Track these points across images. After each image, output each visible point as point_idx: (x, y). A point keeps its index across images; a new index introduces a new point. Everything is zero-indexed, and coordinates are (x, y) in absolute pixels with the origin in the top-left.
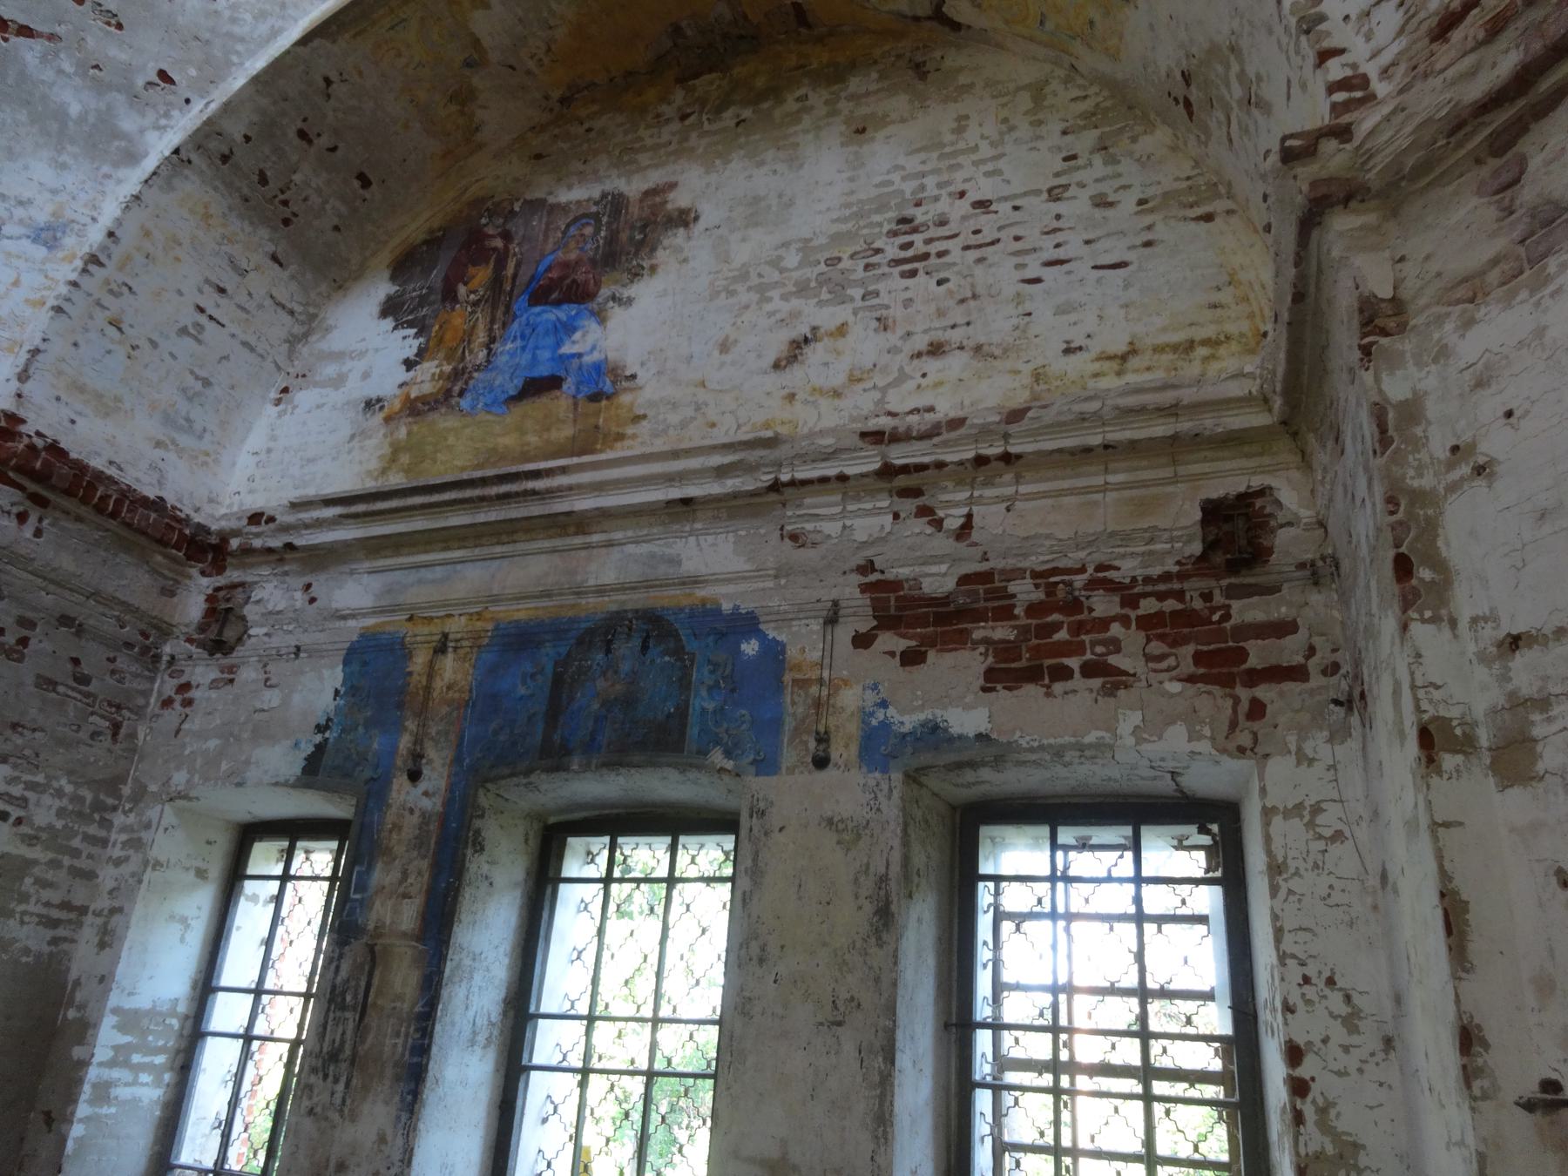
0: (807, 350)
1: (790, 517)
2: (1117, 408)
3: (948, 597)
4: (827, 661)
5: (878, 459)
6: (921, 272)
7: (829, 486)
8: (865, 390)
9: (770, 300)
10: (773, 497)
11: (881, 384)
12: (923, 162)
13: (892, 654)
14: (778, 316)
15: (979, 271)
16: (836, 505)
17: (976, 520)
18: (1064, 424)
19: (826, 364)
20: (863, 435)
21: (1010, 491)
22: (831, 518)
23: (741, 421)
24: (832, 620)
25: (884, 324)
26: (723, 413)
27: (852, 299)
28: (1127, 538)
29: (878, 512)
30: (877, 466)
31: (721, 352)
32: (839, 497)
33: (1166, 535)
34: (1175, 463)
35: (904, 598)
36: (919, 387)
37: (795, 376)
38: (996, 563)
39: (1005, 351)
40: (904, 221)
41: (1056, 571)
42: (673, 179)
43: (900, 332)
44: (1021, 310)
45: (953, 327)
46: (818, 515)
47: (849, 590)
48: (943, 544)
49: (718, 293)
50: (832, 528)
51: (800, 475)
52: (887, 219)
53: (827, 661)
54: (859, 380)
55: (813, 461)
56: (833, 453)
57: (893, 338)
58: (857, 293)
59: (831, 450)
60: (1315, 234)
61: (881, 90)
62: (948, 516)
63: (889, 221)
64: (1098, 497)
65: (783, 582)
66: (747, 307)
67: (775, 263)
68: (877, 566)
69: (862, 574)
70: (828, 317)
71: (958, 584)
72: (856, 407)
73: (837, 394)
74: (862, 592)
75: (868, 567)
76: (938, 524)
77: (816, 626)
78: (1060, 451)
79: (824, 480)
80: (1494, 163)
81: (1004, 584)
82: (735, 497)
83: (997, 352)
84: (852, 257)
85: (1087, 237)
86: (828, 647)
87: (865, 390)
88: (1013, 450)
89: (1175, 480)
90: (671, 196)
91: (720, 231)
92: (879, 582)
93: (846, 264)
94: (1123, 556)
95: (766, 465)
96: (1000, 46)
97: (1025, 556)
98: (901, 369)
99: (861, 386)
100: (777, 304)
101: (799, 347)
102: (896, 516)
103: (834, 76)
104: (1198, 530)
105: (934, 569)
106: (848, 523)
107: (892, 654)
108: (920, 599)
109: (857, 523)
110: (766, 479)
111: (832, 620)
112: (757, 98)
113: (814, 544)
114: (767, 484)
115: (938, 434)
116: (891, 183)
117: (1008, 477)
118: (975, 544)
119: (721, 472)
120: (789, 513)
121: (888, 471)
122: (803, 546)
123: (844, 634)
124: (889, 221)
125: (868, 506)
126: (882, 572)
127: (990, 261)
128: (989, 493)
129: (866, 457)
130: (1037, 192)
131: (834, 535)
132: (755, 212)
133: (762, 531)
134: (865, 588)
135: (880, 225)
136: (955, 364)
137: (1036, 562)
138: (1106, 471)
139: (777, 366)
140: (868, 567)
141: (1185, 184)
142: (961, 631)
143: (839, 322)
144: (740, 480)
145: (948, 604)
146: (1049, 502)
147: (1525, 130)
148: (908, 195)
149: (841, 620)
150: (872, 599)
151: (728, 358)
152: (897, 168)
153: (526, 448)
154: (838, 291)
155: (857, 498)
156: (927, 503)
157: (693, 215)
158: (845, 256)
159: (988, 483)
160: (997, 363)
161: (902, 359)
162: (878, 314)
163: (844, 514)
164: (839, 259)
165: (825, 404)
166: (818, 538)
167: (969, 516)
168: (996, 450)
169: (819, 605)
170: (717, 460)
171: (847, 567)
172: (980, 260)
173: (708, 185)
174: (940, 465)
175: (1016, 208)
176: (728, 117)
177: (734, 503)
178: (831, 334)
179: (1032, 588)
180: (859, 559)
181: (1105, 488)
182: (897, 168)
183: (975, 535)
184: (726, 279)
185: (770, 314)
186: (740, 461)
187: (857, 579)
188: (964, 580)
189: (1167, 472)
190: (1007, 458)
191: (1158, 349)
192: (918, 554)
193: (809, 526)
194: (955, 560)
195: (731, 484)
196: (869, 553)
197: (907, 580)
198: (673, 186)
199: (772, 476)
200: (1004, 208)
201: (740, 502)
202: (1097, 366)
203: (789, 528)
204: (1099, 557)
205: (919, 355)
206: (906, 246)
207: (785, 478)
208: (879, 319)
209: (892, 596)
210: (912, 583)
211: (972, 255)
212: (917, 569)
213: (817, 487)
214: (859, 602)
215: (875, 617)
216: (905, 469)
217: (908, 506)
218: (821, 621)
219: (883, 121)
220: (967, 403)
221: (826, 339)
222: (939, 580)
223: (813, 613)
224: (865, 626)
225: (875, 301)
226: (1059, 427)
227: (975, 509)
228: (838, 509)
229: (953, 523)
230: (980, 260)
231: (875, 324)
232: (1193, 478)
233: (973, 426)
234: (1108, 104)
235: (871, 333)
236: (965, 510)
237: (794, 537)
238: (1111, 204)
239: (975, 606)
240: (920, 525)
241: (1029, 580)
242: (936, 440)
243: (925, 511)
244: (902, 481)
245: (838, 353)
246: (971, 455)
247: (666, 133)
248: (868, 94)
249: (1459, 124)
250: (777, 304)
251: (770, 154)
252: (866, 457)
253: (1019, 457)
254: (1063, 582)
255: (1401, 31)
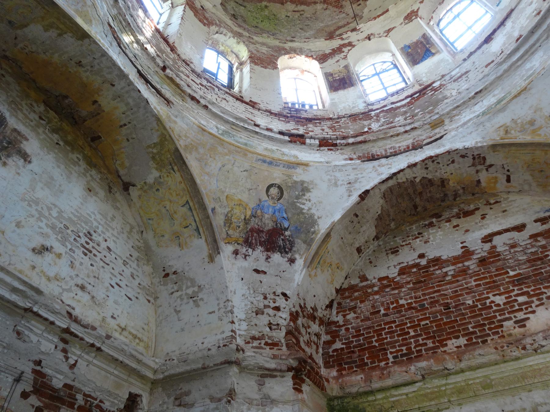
0: (47, 253)
1: (22, 324)
2: (130, 352)
3: (57, 390)
4: (9, 398)
5: (67, 324)
6: (88, 256)
7: (45, 322)
8: (58, 285)
9: (42, 221)
10: (22, 312)
11: (64, 287)
12: (101, 219)
13: (33, 406)
14: (41, 230)
15: (102, 270)
16: (41, 330)
17: (78, 364)
18: (118, 349)
19: (50, 264)
20: (68, 313)
21: (91, 359)
22: (36, 334)
23: (11, 262)
24: (18, 380)
25: (72, 265)
26: (6, 253)
27: (66, 247)
28: (110, 394)
29: (51, 341)
30: (65, 327)
31: (16, 226)
32: (43, 328)
33: (119, 399)
34: (129, 376)
35: (45, 383)
36: (73, 298)
37: (38, 260)
38: (76, 384)
39: (99, 304)
40: (89, 233)
41: (90, 396)
42: (28, 137)
43: (76, 273)
44: (107, 293)
45: (90, 284)
46: (32, 330)
47: (28, 368)
48: (65, 368)
49: (25, 200)
50: (34, 338)
51: (41, 313)
52: (86, 228)
53: (9, 398)
54: (58, 280)
55: (49, 310)
56: (57, 313)
57: (73, 273)
58: (69, 247)
59: (57, 311)
60: (227, 365)
61: (98, 183)
62: (71, 357)
63: (86, 230)
64: (109, 375)
65: (6, 351)
66: (33, 216)
67: (49, 209)
68: (42, 364)
69: (35, 364)
70: (58, 247)
71: (63, 386)
72: (53, 290)
73: (49, 279)
74: (32, 372)
75: (39, 363)
76: (67, 358)
77: (10, 379)
78: (112, 356)
79: (46, 319)
80: (260, 378)
81: (74, 393)
82: (8, 302)
83: (97, 303)
84: (72, 231)
85: (128, 284)
86: (12, 392)
87: (58, 285)
88: (103, 348)
89: (126, 381)
90: (25, 142)
91: (36, 176)
92: (39, 371)
93: (69, 231)
94: (107, 400)
95: (32, 300)
96: (130, 206)
97: (85, 386)
98: (71, 286)
99: (57, 283)
100: (42, 225)
101: (44, 249)
102: (56, 347)
103: (91, 164)
104: (125, 400)
105: (59, 376)
106: (40, 340)
107: (33, 406)
108: (50, 386)
109: (43, 342)
110: (28, 305)
111: (18, 380)
112: (67, 143)
113: (24, 341)
114: (27, 307)
115: (88, 329)
116: (90, 217)
117: (93, 355)
118: (73, 373)
119: (15, 290)
120: (23, 322)
121: (67, 331)
122: (20, 339)
123: (20, 388)
124: (86, 230)
125: (51, 338)
126: (42, 367)
127: (105, 270)
128: (86, 356)
129: (64, 321)
130: (122, 259)
131: (34, 342)
132: (50, 183)
133: (8, 323)
134: (34, 371)
135: (83, 228)
136: (85, 298)
137: (86, 390)
138: (115, 369)
139: (33, 250)
140: (39, 363)
141: (148, 287)
142: (57, 407)
143: (60, 252)
144: (18, 298)
145: (55, 392)
146: (98, 369)
147: (267, 377)
148: (94, 226)
149: (21, 381)
150: (34, 377)
151: (18, 231)
152: (94, 214)
153: (271, 406)
154: (63, 241)
155: (49, 333)
156: (67, 348)
157: (29, 159)
158: (71, 229)
159: (87, 353)
160: (96, 306)
161: (72, 283)
162: (72, 260)
163: (41, 336)
164: (68, 229)
165: (44, 279)
166: (27, 339)
167: (76, 361)
168: (98, 345)
169: (15, 370)
170: (16, 284)
171: (31, 359)
172: (103, 267)
173: (39, 154)
174: (82, 339)
175: (116, 258)
176: (55, 137)
177: (6, 304)
178: (56, 254)
179: (82, 399)
180: (37, 358)
181: (112, 374)
182: (94, 214)
183: (75, 370)
184: (30, 198)
185: (40, 228)
186: (25, 292)
187: (32, 365)
188: (66, 385)
189: (125, 377)
190: (99, 349)
191: (130, 333)
192: (57, 367)
193: (26, 332)
194: (66, 376)
195: (14, 297)
196: (42, 357)
197: (48, 376)
198: (27, 139)
199: (30, 305)
200: (114, 256)
201: (8, 305)
202: (116, 327)
203: (19, 328)
204: (101, 397)
205: (78, 286)
206: (88, 243)
207: (35, 309)
208: (71, 262)
209: (41, 379)
210: (49, 378)
211: (102, 264)
212: (54, 373)
213: (41, 320)
214: (29, 377)
215: (33, 387)
216: (72, 334)
217: (61, 345)
218: (14, 378)
219: (96, 194)
220: (84, 315)
221: (53, 255)
222: (58, 382)
223: (11, 373)
224: (29, 389)
225: (72, 254)
226: (116, 349)
227: (79, 360)
228: (39, 332)
229: (72, 361)
230: (103, 267)
231: (69, 263)
232: (131, 383)
233: (98, 333)
234: (142, 248)
235: (68, 265)
236: (76, 358)
237: (18, 333)
238: (134, 278)
239: (64, 398)
240: (61, 355)
241: (82, 396)
242: (86, 330)
243: (65, 351)
244: (67, 336)
245: (55, 264)
246: (92, 342)
247: (32, 116)
248: (96, 180)
249: (261, 368)
250: (42, 225)
251: (63, 167)
252: (64, 321)
253: (102, 351)
254: (91, 401)
255: (245, 331)
